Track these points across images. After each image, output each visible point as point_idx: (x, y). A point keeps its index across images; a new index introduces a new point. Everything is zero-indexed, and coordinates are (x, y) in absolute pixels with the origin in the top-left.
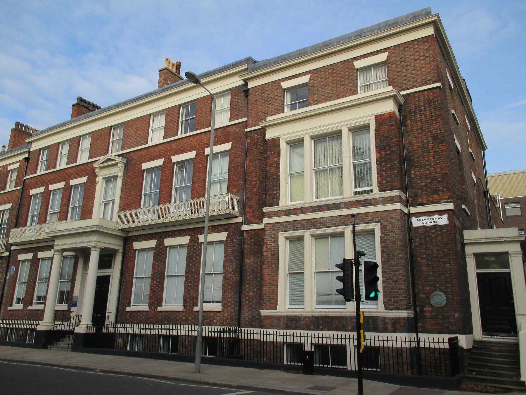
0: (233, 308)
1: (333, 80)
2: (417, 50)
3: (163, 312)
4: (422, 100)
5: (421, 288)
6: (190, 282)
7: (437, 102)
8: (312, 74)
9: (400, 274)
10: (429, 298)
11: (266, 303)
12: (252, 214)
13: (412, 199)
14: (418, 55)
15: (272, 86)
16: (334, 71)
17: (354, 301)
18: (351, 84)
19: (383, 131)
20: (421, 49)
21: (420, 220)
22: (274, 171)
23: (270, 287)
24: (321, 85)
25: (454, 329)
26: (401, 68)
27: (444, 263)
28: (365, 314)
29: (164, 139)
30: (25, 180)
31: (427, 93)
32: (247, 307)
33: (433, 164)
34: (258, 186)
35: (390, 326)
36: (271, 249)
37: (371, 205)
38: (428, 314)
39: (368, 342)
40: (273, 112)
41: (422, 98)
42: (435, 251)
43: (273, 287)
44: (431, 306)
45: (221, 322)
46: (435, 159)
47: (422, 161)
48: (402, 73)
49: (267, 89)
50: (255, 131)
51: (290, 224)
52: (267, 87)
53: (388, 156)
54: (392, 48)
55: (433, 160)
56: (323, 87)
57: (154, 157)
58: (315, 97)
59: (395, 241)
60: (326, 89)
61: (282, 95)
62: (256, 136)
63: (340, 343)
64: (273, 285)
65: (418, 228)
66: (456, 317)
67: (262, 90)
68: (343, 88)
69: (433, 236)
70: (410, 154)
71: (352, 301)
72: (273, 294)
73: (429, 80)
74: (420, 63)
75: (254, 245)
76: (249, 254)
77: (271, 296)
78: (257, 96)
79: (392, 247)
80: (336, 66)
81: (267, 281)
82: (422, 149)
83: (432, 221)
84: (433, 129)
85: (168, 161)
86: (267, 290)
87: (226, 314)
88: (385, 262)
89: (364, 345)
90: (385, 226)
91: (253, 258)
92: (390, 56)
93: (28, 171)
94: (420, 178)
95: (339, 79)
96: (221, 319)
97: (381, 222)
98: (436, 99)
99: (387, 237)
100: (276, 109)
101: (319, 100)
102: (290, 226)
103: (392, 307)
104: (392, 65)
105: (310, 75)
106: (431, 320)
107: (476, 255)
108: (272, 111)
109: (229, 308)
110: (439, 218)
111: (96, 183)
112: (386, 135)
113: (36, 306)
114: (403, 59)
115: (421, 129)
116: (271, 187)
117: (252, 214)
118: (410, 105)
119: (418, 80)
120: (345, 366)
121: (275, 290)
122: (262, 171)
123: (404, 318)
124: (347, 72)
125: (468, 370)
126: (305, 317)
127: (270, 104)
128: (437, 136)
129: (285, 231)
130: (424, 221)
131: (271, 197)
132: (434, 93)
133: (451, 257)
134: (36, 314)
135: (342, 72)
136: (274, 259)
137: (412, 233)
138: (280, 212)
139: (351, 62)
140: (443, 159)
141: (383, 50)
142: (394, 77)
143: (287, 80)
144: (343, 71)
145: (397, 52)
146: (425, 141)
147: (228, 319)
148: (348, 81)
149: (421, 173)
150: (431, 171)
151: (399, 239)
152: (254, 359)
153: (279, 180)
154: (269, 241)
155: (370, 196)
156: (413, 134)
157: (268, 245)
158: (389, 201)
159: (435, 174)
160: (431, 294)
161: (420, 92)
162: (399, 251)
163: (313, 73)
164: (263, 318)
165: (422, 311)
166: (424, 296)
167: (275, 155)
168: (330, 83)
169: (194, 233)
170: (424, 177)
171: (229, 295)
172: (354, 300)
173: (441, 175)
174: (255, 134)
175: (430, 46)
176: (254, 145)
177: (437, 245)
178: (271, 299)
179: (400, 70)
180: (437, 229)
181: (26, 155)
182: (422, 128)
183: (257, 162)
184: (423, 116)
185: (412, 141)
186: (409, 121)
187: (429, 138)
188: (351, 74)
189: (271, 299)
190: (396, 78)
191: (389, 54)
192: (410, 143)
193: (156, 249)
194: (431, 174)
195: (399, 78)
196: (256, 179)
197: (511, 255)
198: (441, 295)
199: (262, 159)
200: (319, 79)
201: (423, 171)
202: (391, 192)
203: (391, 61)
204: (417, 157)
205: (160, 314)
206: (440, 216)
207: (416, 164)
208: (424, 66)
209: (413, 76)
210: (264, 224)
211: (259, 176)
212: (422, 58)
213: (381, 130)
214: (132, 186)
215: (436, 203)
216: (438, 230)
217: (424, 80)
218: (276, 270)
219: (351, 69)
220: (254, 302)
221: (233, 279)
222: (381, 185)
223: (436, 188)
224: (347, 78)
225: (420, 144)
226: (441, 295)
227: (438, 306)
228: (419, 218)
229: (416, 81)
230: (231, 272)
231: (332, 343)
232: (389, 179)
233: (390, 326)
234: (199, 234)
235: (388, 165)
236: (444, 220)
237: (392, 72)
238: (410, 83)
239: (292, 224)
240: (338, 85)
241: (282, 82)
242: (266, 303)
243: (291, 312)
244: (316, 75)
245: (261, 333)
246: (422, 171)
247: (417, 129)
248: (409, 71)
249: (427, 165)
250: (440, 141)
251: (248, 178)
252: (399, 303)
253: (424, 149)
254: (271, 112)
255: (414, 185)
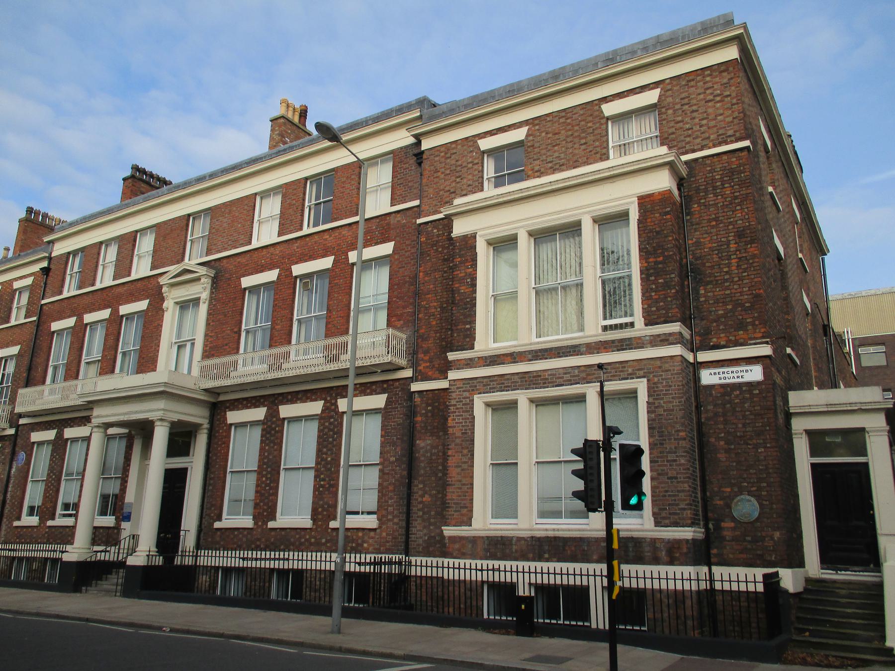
0: (397, 524)
1: (567, 137)
2: (710, 85)
3: (278, 530)
4: (719, 169)
5: (716, 489)
6: (324, 480)
7: (744, 173)
8: (531, 126)
9: (681, 465)
10: (729, 507)
11: (453, 515)
12: (428, 364)
13: (700, 338)
14: (712, 94)
15: (463, 146)
16: (569, 121)
17: (602, 512)
18: (597, 143)
19: (651, 222)
20: (717, 83)
21: (715, 374)
22: (466, 291)
23: (460, 488)
24: (547, 145)
25: (773, 559)
26: (682, 115)
27: (756, 447)
28: (620, 533)
29: (279, 236)
30: (42, 305)
31: (726, 157)
32: (421, 522)
33: (736, 279)
34: (438, 316)
35: (664, 553)
36: (462, 423)
37: (632, 349)
38: (727, 534)
39: (627, 581)
40: (465, 189)
41: (718, 166)
42: (740, 426)
43: (465, 488)
44: (733, 519)
45: (377, 547)
46: (740, 271)
47: (719, 274)
48: (684, 124)
49: (455, 151)
50: (433, 223)
51: (493, 381)
52: (454, 149)
53: (660, 266)
54: (668, 81)
55: (736, 271)
56: (549, 147)
57: (262, 266)
58: (537, 165)
59: (673, 410)
60: (555, 152)
61: (480, 162)
62: (435, 231)
63: (578, 583)
64: (464, 484)
65: (711, 387)
66: (776, 538)
67: (446, 153)
68: (584, 150)
69: (736, 401)
70: (698, 262)
71: (599, 511)
72: (465, 500)
73: (730, 136)
74: (715, 106)
75: (432, 416)
76: (423, 431)
77: (461, 503)
78: (438, 163)
79: (666, 420)
80: (572, 112)
81: (454, 477)
82: (718, 253)
83: (735, 375)
84: (736, 219)
85: (286, 274)
86: (453, 492)
87: (384, 534)
88: (656, 444)
89: (620, 587)
90: (654, 383)
91: (431, 438)
92: (663, 95)
93: (47, 290)
94: (715, 303)
95: (576, 134)
96: (376, 542)
97: (648, 377)
98: (742, 168)
99: (659, 403)
100: (469, 185)
101: (542, 170)
102: (494, 384)
103: (667, 521)
104: (667, 110)
105: (527, 128)
106: (734, 543)
107: (810, 433)
108: (463, 188)
109: (390, 524)
110: (747, 371)
111: (163, 311)
112: (657, 229)
113: (61, 520)
114: (686, 101)
115: (716, 219)
116: (461, 317)
117: (428, 364)
118: (698, 178)
119: (712, 136)
120: (587, 621)
121: (467, 492)
122: (446, 291)
123: (687, 541)
124: (590, 122)
125: (796, 629)
126: (519, 539)
127: (460, 176)
128: (743, 230)
129: (484, 393)
130: (722, 376)
131: (461, 334)
132: (739, 158)
133: (768, 437)
134: (61, 533)
135: (583, 123)
136: (467, 441)
137: (701, 396)
138: (476, 359)
139: (596, 105)
140: (754, 270)
141: (651, 86)
142: (671, 131)
143: (489, 135)
144: (583, 120)
145: (675, 88)
146: (723, 239)
147: (388, 542)
148: (592, 138)
149: (716, 293)
150: (733, 291)
151: (678, 406)
152: (432, 610)
153: (475, 305)
154: (457, 409)
155: (629, 334)
156: (702, 227)
157: (457, 416)
158: (661, 341)
159: (741, 295)
160: (733, 499)
161: (715, 157)
162: (678, 427)
163: (532, 123)
164: (447, 541)
165: (718, 528)
166: (721, 503)
167: (468, 264)
168: (562, 141)
169: (331, 396)
170: (721, 301)
171: (390, 501)
172: (603, 509)
173: (750, 297)
174: (434, 227)
175: (732, 78)
176: (432, 246)
177: (744, 416)
178: (461, 507)
179: (680, 118)
180: (744, 388)
181: (45, 264)
182: (719, 217)
183: (438, 275)
184: (719, 197)
185: (702, 240)
186: (696, 206)
187: (730, 235)
188: (598, 125)
189: (461, 507)
190: (673, 133)
191: (663, 92)
192: (698, 244)
193: (266, 424)
194: (733, 295)
195: (679, 132)
196: (436, 304)
197: (870, 434)
198: (750, 501)
199: (445, 269)
200: (543, 134)
201: (720, 290)
202: (666, 327)
203: (665, 103)
204: (709, 267)
205: (273, 533)
206: (748, 368)
207: (708, 279)
208: (721, 111)
209: (703, 129)
210: (449, 380)
211: (440, 298)
212: (718, 99)
213: (649, 220)
214: (225, 316)
215: (742, 345)
216: (745, 391)
217: (722, 137)
218: (469, 459)
219: (596, 117)
220: (433, 513)
221: (396, 473)
222: (648, 315)
223: (742, 319)
224: (591, 133)
225: (715, 245)
226: (750, 501)
227: (746, 520)
228: (713, 371)
229: (709, 138)
230: (393, 462)
231: (565, 582)
232: (661, 304)
233: (663, 554)
234: (339, 397)
235: (660, 281)
236: (755, 374)
237: (667, 122)
238: (698, 140)
239: (497, 380)
240: (575, 144)
241: (479, 139)
242: (453, 515)
243: (495, 530)
244: (537, 127)
245: (444, 566)
246: (718, 290)
247: (709, 219)
248: (697, 120)
249: (727, 280)
250: (749, 239)
251: (422, 303)
252: (678, 514)
253: (721, 253)
254: (462, 190)
255: (705, 313)
